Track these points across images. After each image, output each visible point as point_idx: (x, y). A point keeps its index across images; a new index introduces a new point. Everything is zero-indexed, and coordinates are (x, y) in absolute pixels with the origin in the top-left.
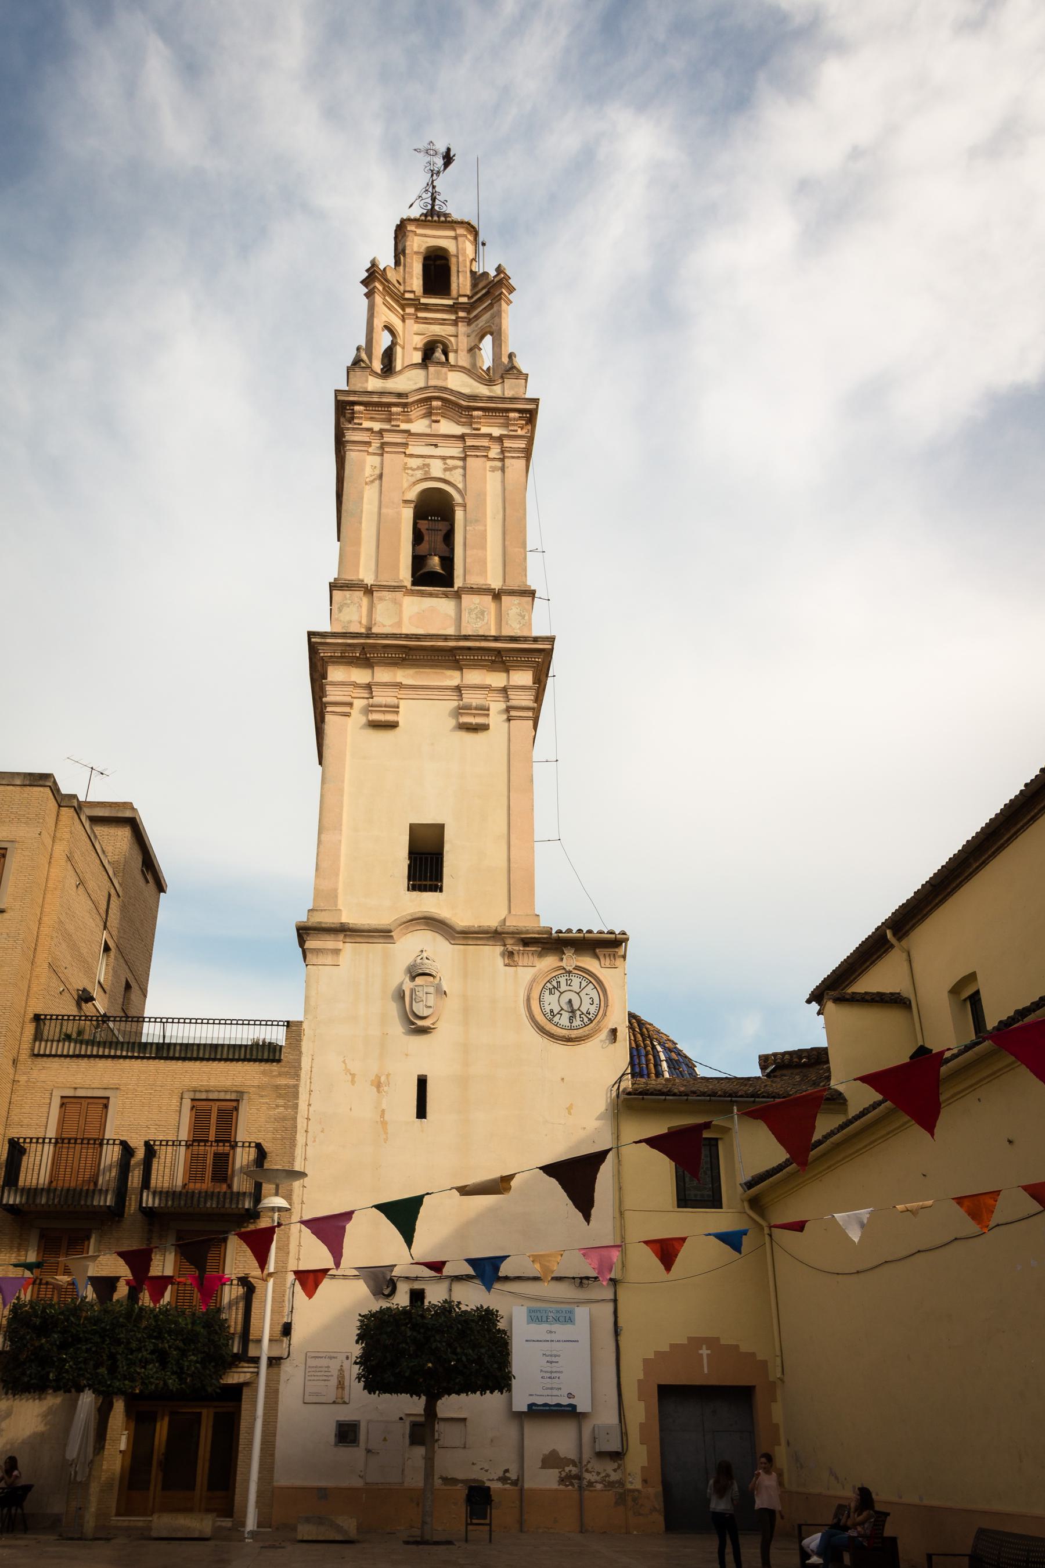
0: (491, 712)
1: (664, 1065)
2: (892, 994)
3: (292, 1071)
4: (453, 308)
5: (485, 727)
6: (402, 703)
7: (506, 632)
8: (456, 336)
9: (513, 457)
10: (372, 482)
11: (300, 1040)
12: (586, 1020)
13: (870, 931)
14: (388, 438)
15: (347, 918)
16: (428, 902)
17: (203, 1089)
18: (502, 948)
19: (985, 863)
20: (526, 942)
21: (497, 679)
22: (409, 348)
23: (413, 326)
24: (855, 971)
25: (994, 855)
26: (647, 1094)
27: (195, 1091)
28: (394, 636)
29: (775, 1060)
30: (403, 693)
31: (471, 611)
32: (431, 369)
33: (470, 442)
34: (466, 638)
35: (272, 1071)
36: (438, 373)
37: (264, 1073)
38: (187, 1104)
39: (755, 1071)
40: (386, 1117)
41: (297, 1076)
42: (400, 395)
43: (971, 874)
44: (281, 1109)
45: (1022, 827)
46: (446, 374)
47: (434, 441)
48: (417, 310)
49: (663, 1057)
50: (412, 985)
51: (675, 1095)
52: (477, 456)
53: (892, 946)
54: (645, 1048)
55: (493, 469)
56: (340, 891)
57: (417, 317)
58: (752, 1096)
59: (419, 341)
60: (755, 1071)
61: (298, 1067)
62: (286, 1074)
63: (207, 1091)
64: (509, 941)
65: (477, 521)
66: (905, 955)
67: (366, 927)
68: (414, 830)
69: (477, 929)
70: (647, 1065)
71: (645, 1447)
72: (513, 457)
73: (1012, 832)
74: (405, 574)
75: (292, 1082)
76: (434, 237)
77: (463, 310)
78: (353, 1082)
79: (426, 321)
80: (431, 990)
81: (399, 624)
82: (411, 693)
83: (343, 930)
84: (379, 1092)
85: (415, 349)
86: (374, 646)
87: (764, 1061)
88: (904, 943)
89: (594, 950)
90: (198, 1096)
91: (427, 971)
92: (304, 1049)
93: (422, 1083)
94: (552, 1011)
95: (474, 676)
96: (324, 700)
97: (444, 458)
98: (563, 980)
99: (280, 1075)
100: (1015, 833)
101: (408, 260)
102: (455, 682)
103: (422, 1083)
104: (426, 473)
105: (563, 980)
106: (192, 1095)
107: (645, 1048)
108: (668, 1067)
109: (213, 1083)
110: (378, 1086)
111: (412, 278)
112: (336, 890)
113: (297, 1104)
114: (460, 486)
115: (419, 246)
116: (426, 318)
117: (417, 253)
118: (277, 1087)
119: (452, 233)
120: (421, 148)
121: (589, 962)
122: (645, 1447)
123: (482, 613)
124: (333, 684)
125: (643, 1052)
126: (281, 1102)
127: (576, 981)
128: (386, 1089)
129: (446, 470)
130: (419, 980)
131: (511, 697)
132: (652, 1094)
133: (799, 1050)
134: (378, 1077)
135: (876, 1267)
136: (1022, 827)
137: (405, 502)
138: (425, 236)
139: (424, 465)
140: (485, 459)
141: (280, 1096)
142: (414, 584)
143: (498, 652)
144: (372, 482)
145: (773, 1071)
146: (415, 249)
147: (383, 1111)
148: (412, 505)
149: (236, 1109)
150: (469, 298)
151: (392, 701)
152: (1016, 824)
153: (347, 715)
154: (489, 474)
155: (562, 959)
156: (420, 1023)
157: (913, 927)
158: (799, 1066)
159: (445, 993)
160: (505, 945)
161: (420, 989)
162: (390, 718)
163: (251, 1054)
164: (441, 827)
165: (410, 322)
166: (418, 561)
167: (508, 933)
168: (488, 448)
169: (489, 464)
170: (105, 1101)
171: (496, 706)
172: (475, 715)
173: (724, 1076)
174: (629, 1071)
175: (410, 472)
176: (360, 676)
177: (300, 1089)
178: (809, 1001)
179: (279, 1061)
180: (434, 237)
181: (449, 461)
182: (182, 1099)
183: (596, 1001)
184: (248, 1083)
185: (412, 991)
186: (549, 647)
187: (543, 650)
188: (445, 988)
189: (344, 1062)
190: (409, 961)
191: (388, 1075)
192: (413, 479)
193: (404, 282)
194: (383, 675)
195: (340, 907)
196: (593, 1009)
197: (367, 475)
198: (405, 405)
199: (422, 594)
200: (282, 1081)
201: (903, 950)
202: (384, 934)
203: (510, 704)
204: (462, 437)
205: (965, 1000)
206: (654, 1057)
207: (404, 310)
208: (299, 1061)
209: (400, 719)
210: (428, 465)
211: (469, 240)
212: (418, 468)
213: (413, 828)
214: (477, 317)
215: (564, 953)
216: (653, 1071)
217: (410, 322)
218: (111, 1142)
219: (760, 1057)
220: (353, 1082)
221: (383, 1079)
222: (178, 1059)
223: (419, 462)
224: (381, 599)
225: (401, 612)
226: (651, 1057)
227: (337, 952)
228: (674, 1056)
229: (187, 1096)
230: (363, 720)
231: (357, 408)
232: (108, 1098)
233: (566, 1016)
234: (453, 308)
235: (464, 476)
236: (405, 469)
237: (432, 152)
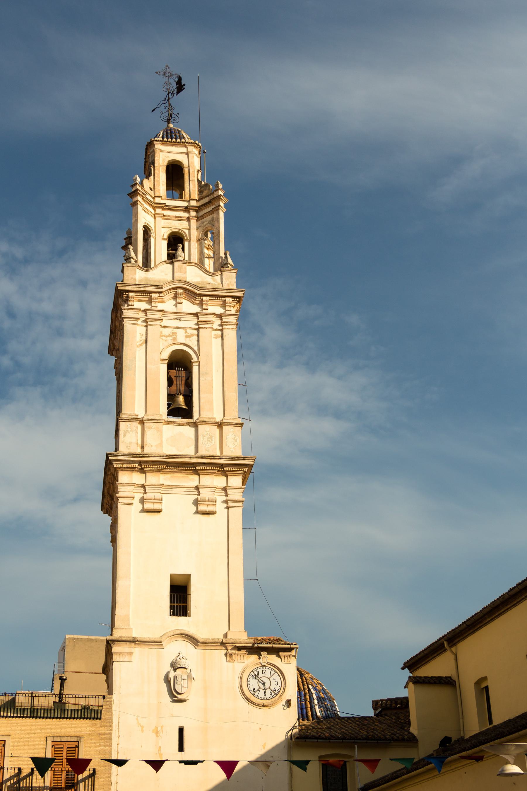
0: (217, 503)
1: (316, 702)
2: (446, 677)
3: (108, 724)
4: (187, 209)
5: (213, 513)
6: (164, 497)
7: (226, 453)
8: (189, 229)
9: (229, 329)
10: (141, 345)
11: (111, 707)
12: (273, 694)
13: (436, 639)
14: (150, 315)
15: (135, 634)
16: (181, 623)
17: (58, 735)
18: (226, 651)
19: (493, 620)
20: (239, 648)
21: (219, 481)
22: (159, 238)
23: (162, 222)
24: (429, 657)
25: (498, 617)
26: (307, 738)
27: (54, 736)
28: (160, 456)
29: (381, 705)
30: (163, 490)
31: (204, 436)
32: (176, 265)
33: (202, 318)
34: (202, 457)
35: (96, 725)
36: (180, 268)
37: (92, 725)
38: (50, 744)
39: (370, 712)
40: (162, 751)
41: (111, 727)
42: (157, 286)
43: (486, 623)
44: (103, 747)
45: (510, 608)
46: (185, 268)
47: (179, 316)
49: (315, 697)
50: (175, 674)
51: (323, 738)
52: (206, 328)
53: (445, 650)
54: (304, 691)
55: (216, 337)
56: (131, 616)
58: (366, 739)
59: (166, 233)
60: (370, 712)
61: (111, 722)
62: (105, 726)
63: (60, 736)
64: (230, 648)
65: (207, 374)
66: (453, 657)
67: (147, 640)
68: (172, 577)
69: (211, 641)
70: (305, 702)
72: (229, 329)
73: (505, 609)
74: (164, 410)
75: (108, 731)
76: (173, 153)
77: (193, 210)
78: (142, 731)
79: (169, 218)
80: (186, 677)
81: (161, 445)
82: (170, 490)
83: (133, 641)
84: (157, 736)
85: (163, 239)
86: (147, 462)
87: (376, 704)
88: (453, 649)
89: (278, 653)
90: (55, 739)
91: (183, 666)
92: (114, 712)
93: (181, 730)
94: (254, 689)
95: (207, 480)
96: (117, 495)
97: (185, 329)
98: (260, 671)
99: (101, 727)
100: (507, 609)
102: (196, 483)
103: (181, 730)
104: (175, 339)
105: (260, 671)
106: (52, 739)
107: (304, 691)
108: (318, 703)
109: (63, 732)
110: (157, 733)
111: (159, 185)
112: (128, 615)
113: (111, 744)
114: (196, 348)
115: (163, 160)
117: (162, 166)
118: (100, 734)
119: (184, 150)
120: (160, 71)
121: (273, 659)
123: (211, 437)
124: (122, 485)
125: (303, 694)
126: (102, 742)
127: (268, 671)
128: (161, 734)
129: (187, 337)
130: (179, 671)
131: (229, 493)
132: (310, 738)
133: (396, 698)
134: (156, 728)
136: (510, 608)
137: (162, 360)
138: (167, 152)
139: (173, 333)
140: (211, 330)
141: (101, 739)
142: (169, 414)
143: (222, 466)
144: (141, 345)
145: (380, 712)
146: (161, 162)
147: (160, 747)
148: (166, 362)
149: (78, 747)
150: (198, 201)
151: (158, 496)
152: (506, 606)
153: (131, 504)
154: (214, 340)
155: (260, 658)
156: (180, 697)
157: (459, 642)
158: (396, 708)
159: (194, 679)
160: (227, 650)
161: (180, 677)
162: (156, 506)
163: (84, 715)
164: (189, 575)
166: (171, 397)
167: (229, 643)
168: (212, 323)
169: (214, 332)
170: (3, 742)
171: (220, 498)
172: (207, 505)
173: (352, 716)
174: (297, 724)
175: (164, 338)
176: (138, 478)
177: (113, 735)
178: (403, 668)
179: (100, 719)
180: (173, 153)
181: (188, 331)
182: (46, 741)
183: (279, 683)
184: (83, 731)
185: (174, 677)
186: (252, 463)
187: (249, 465)
188: (193, 676)
189: (137, 719)
190: (172, 658)
191: (162, 727)
192: (166, 344)
193: (154, 188)
194: (152, 478)
195: (131, 626)
196: (277, 688)
197: (138, 339)
198: (160, 293)
199: (174, 423)
200: (103, 730)
201: (452, 652)
202: (158, 643)
203: (228, 498)
204: (196, 315)
205: (483, 688)
206: (310, 697)
207: (155, 210)
208: (111, 718)
209: (163, 507)
210: (175, 334)
211: (196, 155)
212: (169, 336)
213: (171, 576)
215: (261, 655)
216: (309, 706)
218: (9, 769)
219: (373, 701)
220: (142, 731)
221: (159, 729)
222: (43, 718)
223: (170, 331)
224: (149, 428)
225: (161, 437)
226: (308, 697)
227: (131, 654)
228: (322, 695)
229: (50, 740)
230: (140, 507)
231: (130, 294)
232: (5, 741)
233: (262, 692)
234: (187, 209)
235: (198, 341)
236: (161, 336)
237: (168, 74)
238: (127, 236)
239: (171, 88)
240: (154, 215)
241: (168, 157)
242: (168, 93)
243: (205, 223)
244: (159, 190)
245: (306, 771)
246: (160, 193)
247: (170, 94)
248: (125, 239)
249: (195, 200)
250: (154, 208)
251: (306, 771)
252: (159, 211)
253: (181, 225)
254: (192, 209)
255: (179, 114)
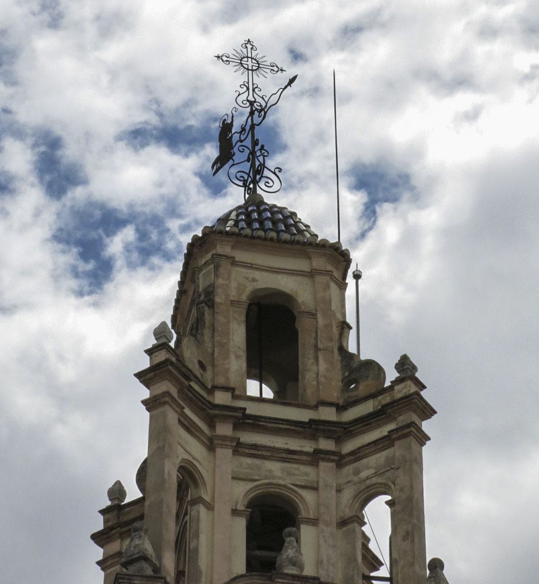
22: (223, 508)
48: (236, 427)
57: (239, 444)
59: (240, 492)
71: (347, 281)
79: (256, 451)
85: (235, 512)
101: (220, 318)
111: (226, 357)
115: (241, 288)
116: (255, 446)
122: (347, 281)
135: (183, 448)
138: (251, 266)
146: (233, 294)
165: (224, 454)
207: (212, 425)
214: (358, 455)
217: (224, 454)
237: (250, 64)
238: (109, 503)
239: (259, 99)
240: (211, 440)
241: (254, 280)
242: (252, 113)
243: (363, 475)
244: (227, 370)
245: (136, 375)
246: (228, 378)
247: (256, 113)
248: (103, 512)
249: (331, 404)
250: (211, 422)
251: (136, 375)
252: (224, 429)
253: (290, 474)
254: (323, 431)
255: (280, 170)
